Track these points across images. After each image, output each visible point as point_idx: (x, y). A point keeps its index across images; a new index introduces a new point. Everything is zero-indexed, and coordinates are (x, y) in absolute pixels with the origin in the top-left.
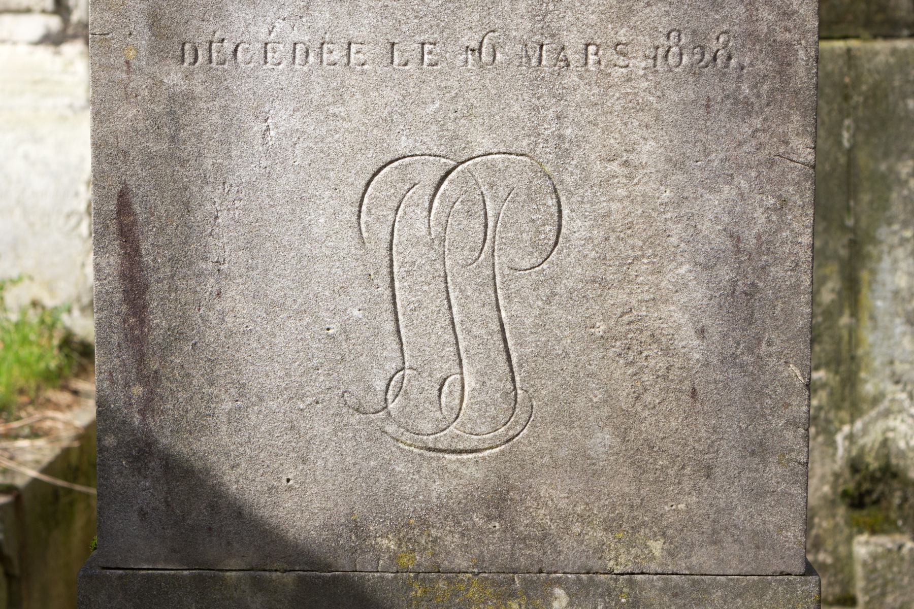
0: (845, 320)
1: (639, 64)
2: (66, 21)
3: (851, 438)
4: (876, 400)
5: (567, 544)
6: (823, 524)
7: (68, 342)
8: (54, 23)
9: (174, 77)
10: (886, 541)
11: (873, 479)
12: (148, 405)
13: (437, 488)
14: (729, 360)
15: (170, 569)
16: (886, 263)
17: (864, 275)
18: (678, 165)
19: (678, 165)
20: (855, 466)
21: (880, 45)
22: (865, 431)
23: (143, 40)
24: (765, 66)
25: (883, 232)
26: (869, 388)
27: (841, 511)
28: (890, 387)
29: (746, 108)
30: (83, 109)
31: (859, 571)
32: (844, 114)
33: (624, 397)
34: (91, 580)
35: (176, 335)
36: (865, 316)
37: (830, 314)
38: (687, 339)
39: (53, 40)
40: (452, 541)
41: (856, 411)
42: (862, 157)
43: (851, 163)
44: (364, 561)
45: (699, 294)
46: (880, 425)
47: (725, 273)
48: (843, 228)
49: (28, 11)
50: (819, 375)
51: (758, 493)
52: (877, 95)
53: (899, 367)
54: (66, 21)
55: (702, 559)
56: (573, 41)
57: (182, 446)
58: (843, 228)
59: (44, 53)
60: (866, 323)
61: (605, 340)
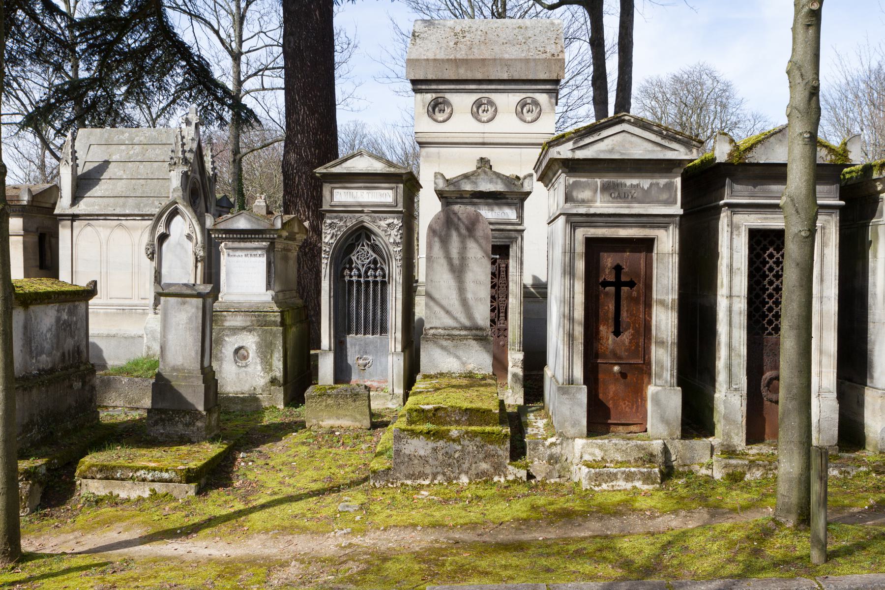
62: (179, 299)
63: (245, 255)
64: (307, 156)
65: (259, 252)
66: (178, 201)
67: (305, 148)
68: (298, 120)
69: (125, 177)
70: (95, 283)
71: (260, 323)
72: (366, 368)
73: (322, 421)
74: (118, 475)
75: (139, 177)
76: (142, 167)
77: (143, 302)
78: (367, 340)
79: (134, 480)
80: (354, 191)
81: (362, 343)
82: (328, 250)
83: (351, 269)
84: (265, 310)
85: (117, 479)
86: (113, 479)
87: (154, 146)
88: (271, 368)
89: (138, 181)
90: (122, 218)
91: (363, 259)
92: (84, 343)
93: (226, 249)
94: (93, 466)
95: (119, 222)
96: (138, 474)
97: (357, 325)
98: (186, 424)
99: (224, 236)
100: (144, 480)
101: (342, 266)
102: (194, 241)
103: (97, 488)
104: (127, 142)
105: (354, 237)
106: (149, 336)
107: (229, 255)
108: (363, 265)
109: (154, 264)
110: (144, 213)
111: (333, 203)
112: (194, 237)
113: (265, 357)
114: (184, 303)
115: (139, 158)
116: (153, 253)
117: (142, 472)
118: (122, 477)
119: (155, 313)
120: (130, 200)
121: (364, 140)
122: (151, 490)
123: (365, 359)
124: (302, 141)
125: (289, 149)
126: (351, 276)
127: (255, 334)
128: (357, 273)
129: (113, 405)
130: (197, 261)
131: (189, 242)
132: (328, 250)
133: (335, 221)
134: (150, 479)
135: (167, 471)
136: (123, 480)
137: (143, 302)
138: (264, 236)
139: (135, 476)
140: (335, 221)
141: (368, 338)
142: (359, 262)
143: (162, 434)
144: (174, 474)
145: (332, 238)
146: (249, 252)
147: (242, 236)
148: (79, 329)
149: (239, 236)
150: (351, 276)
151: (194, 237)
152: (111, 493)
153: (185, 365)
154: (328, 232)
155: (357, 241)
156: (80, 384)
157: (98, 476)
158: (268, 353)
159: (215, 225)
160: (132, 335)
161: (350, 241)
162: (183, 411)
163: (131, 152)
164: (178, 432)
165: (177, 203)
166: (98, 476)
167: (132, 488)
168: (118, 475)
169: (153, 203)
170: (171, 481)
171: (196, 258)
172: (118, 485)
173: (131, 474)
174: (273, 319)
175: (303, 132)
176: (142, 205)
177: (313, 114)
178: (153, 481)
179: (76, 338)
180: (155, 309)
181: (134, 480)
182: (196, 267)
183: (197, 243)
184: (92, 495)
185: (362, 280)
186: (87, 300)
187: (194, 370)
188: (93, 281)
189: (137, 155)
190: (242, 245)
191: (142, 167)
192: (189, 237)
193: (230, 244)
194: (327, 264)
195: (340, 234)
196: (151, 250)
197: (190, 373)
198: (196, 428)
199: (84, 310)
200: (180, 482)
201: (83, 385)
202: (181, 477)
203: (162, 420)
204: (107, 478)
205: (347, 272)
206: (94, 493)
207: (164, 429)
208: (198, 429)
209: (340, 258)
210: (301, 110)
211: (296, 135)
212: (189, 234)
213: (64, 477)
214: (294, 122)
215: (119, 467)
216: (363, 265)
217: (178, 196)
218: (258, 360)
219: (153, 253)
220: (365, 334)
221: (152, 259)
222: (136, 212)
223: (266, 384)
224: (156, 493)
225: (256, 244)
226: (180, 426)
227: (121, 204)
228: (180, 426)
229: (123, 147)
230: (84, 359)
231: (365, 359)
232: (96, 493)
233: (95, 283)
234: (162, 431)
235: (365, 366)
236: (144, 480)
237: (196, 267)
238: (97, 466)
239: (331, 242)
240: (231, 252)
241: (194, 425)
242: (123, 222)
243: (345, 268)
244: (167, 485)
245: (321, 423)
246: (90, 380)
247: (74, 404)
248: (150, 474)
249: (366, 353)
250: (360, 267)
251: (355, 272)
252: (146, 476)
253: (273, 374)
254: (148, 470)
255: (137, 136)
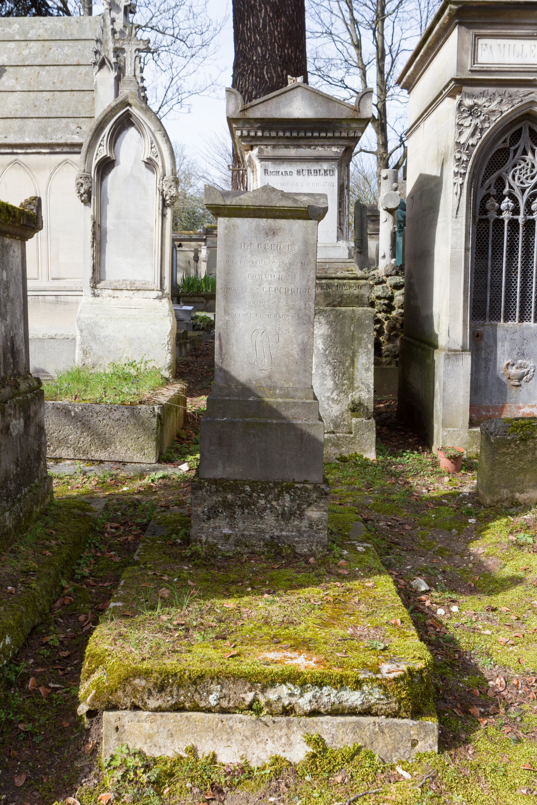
0: (351, 369)
1: (290, 318)
2: (163, 293)
3: (352, 396)
4: (358, 388)
5: (279, 383)
6: (346, 415)
7: (163, 377)
8: (160, 293)
9: (227, 318)
10: (359, 419)
11: (357, 405)
12: (222, 363)
13: (261, 375)
14: (302, 358)
15: (225, 385)
16: (360, 357)
17: (356, 360)
18: (295, 331)
19: (295, 331)
20: (353, 403)
21: (360, 308)
22: (355, 395)
23: (223, 313)
24: (307, 318)
25: (360, 350)
26: (356, 385)
27: (350, 412)
28: (361, 385)
29: (304, 324)
30: (464, 350)
31: (353, 426)
32: (352, 324)
33: (287, 363)
34: (14, 620)
35: (226, 353)
36: (355, 369)
37: (348, 368)
38: (296, 355)
39: (160, 298)
40: (263, 382)
41: (353, 390)
42: (356, 333)
43: (353, 335)
44: (251, 385)
45: (298, 349)
46: (359, 393)
47: (301, 346)
48: (351, 349)
49: (153, 290)
50: (345, 382)
51: (305, 377)
52: (359, 319)
53: (363, 380)
54: (163, 293)
55: (297, 386)
56: (281, 314)
57: (226, 369)
58: (351, 349)
59: (157, 301)
60: (356, 370)
61: (285, 355)
62: (263, 222)
63: (298, 172)
64: (271, 79)
65: (325, 166)
66: (131, 101)
67: (269, 67)
68: (256, 27)
69: (18, 88)
70: (37, 202)
71: (330, 300)
72: (522, 382)
73: (522, 492)
74: (212, 700)
75: (42, 88)
76: (44, 73)
77: (56, 284)
78: (526, 332)
79: (258, 711)
80: (518, 43)
81: (517, 336)
82: (465, 158)
83: (500, 198)
84: (339, 274)
85: (209, 710)
86: (196, 708)
87: (62, 43)
88: (352, 383)
89: (40, 94)
90: (19, 151)
91: (523, 178)
92: (21, 332)
93: (262, 159)
94: (137, 674)
95: (14, 157)
96: (272, 695)
97: (507, 301)
98: (283, 514)
99: (260, 134)
100: (287, 711)
101: (484, 192)
102: (160, 171)
103: (150, 737)
104: (17, 38)
105: (508, 135)
106: (85, 333)
107: (266, 171)
108: (523, 191)
109: (89, 211)
110: (54, 141)
111: (476, 67)
112: (160, 164)
113: (342, 363)
114: (273, 232)
115: (39, 61)
116: (89, 193)
117: (283, 690)
118: (224, 704)
119: (94, 295)
120: (30, 122)
121: (185, 161)
122: (309, 742)
123: (521, 367)
124: (264, 56)
125: (244, 70)
126: (500, 212)
127: (323, 321)
128: (511, 204)
129: (53, 455)
130: (164, 205)
131: (150, 173)
132: (465, 158)
133: (480, 101)
134: (308, 708)
135: (358, 684)
136: (224, 711)
137: (56, 284)
138: (337, 134)
139: (263, 700)
140: (480, 101)
141: (528, 328)
142: (516, 184)
143: (227, 537)
144: (377, 694)
145: (473, 135)
146: (305, 166)
147: (295, 134)
148: (12, 301)
149: (288, 134)
150: (500, 212)
151: (160, 164)
152: (193, 751)
153: (277, 376)
154: (467, 124)
155: (512, 144)
156: (22, 421)
157: (153, 703)
158: (346, 355)
159: (244, 110)
160: (40, 336)
161: (499, 145)
162: (276, 484)
163: (26, 52)
164: (263, 531)
165: (129, 105)
166: (153, 703)
167: (255, 735)
168: (212, 700)
169: (67, 126)
170: (367, 712)
171: (164, 200)
172: (210, 729)
173: (249, 697)
174: (356, 292)
175: (265, 44)
176: (49, 130)
177: (279, 17)
178: (315, 713)
179: (8, 318)
180: (94, 287)
181: (258, 711)
182: (164, 215)
183: (165, 175)
184: (137, 761)
185: (521, 218)
186: (24, 239)
187: (296, 390)
188: (35, 198)
189: (36, 56)
190: (292, 152)
191: (44, 73)
192: (150, 164)
193: (269, 151)
194: (462, 185)
195: (489, 127)
196: (85, 187)
197: (287, 395)
198: (305, 523)
199: (19, 260)
200: (396, 715)
201: (25, 423)
202: (400, 701)
203: (228, 506)
204: (178, 708)
205: (491, 203)
206: (140, 753)
207: (231, 527)
208: (311, 526)
209: (481, 177)
210: (261, 11)
211: (253, 48)
212: (150, 159)
213: (31, 683)
214: (249, 29)
215: (216, 677)
216: (523, 191)
217: (132, 93)
218: (328, 370)
219: (89, 193)
220: (521, 320)
221: (87, 201)
222: (42, 140)
223: (342, 414)
224: (325, 750)
225: (320, 151)
226: (270, 519)
227: (17, 129)
228: (270, 519)
229: (12, 45)
230: (22, 371)
231: (521, 367)
232: (151, 752)
233: (37, 202)
234: (226, 531)
235: (520, 379)
236: (287, 711)
237: (164, 215)
238: (147, 673)
239: (471, 142)
240: (270, 166)
241: (301, 516)
242: (21, 158)
243: (487, 197)
244: (358, 725)
245: (517, 495)
246: (36, 414)
247: (12, 467)
248: (308, 696)
249: (523, 355)
250: (517, 193)
251: (506, 203)
252: (294, 700)
253: (355, 395)
254: (303, 685)
255: (33, 28)
